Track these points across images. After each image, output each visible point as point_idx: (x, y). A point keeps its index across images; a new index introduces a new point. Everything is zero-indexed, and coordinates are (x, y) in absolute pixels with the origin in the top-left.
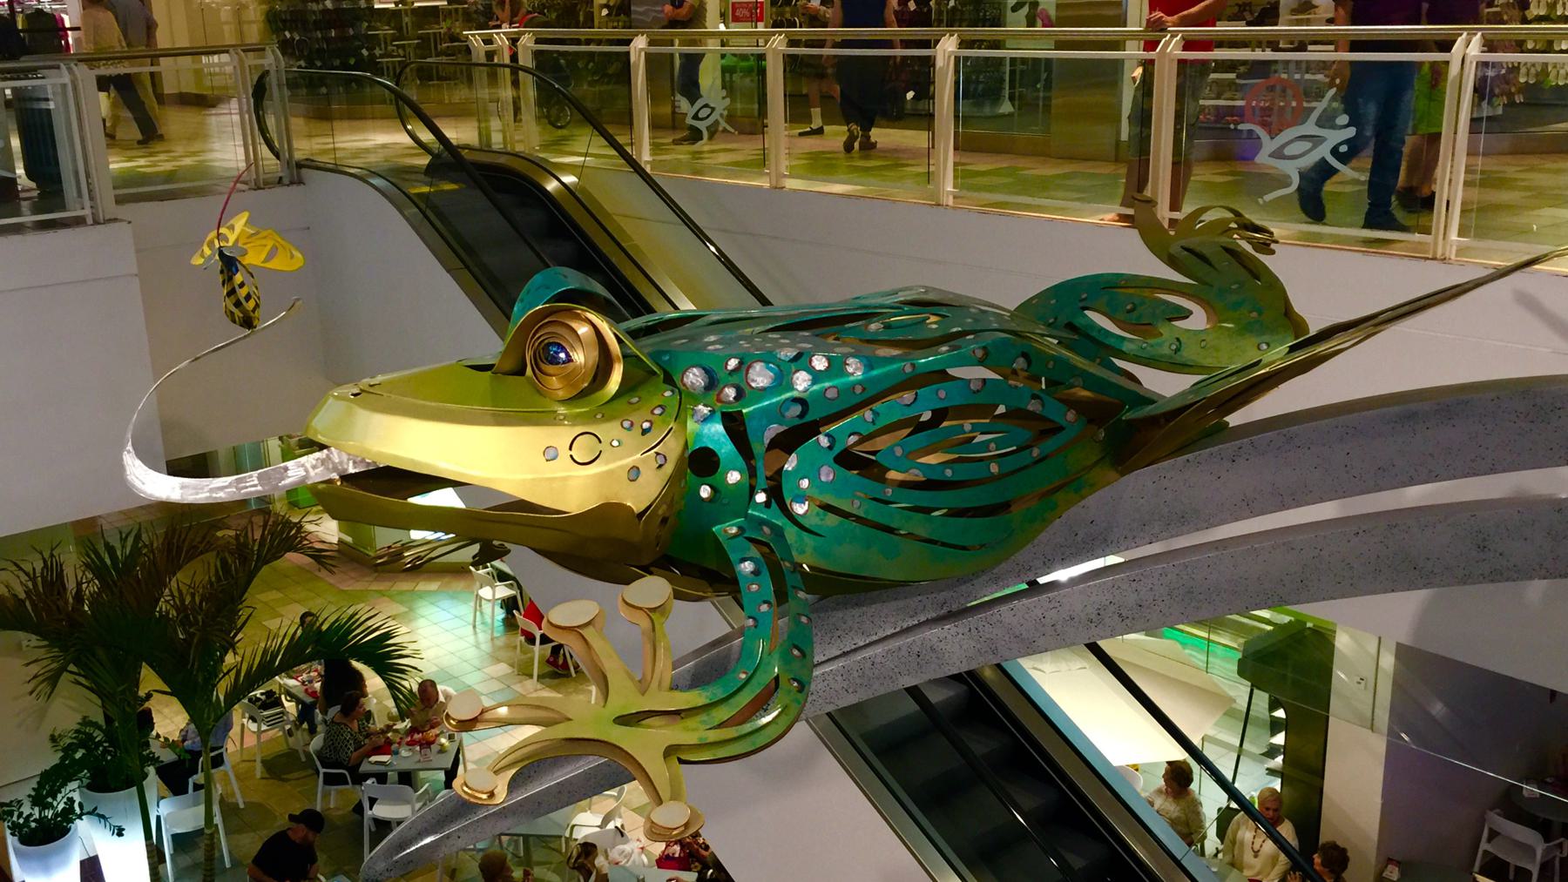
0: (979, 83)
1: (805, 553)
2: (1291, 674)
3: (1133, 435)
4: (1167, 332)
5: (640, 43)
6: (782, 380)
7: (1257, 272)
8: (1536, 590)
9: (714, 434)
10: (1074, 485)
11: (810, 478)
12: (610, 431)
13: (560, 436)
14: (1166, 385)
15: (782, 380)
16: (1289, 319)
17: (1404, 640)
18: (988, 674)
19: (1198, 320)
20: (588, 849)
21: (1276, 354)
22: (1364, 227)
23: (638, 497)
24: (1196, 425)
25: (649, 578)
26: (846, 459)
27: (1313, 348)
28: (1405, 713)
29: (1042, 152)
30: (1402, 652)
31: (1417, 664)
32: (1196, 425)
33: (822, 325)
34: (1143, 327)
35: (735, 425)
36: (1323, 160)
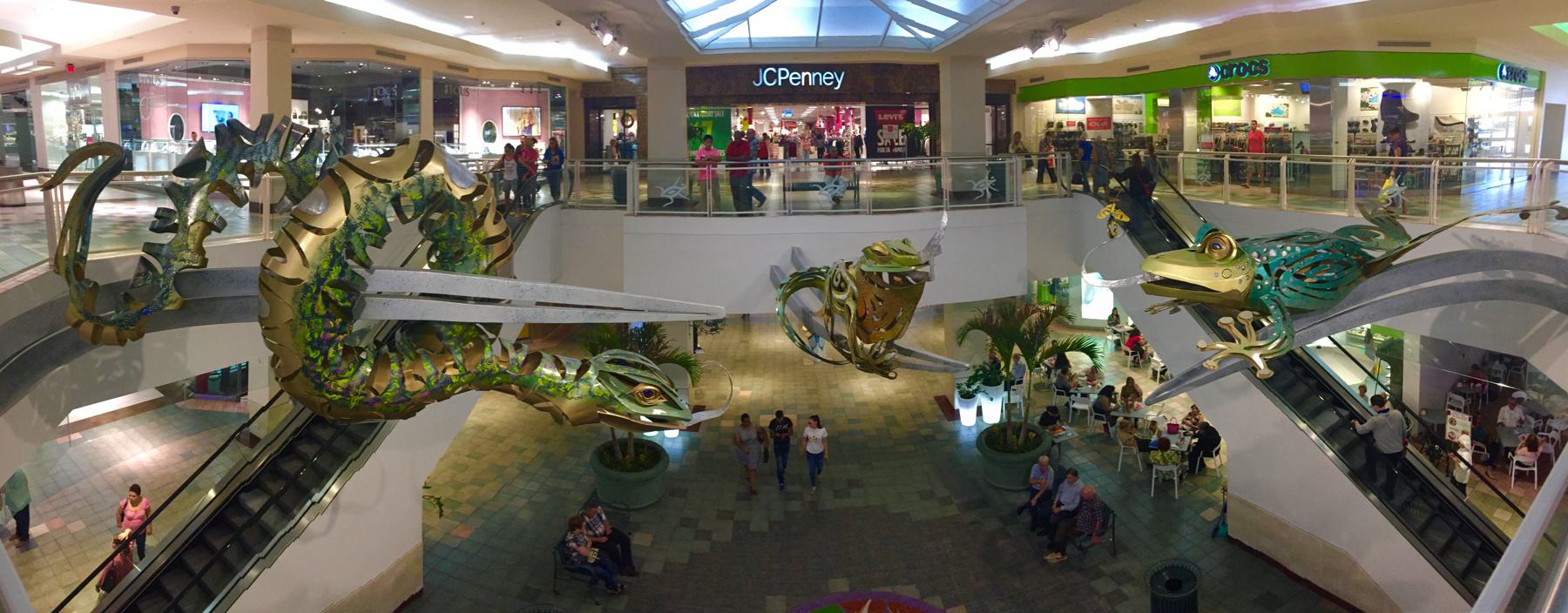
0: (1294, 170)
1: (1286, 302)
2: (1392, 353)
3: (1370, 268)
4: (1374, 240)
5: (1284, 159)
6: (1279, 254)
7: (1397, 224)
8: (1477, 305)
9: (1262, 271)
10: (1356, 282)
11: (1287, 280)
12: (1233, 268)
13: (1220, 270)
14: (1377, 254)
15: (1279, 254)
16: (1407, 236)
17: (1427, 334)
18: (1299, 352)
19: (1382, 236)
21: (1406, 244)
22: (660, 325)
23: (1242, 288)
24: (1384, 265)
25: (411, 540)
26: (1296, 276)
27: (1416, 243)
28: (1424, 359)
29: (1308, 194)
30: (1424, 339)
31: (1431, 345)
32: (1384, 265)
33: (1286, 238)
34: (1367, 239)
35: (1267, 267)
36: (1232, 181)
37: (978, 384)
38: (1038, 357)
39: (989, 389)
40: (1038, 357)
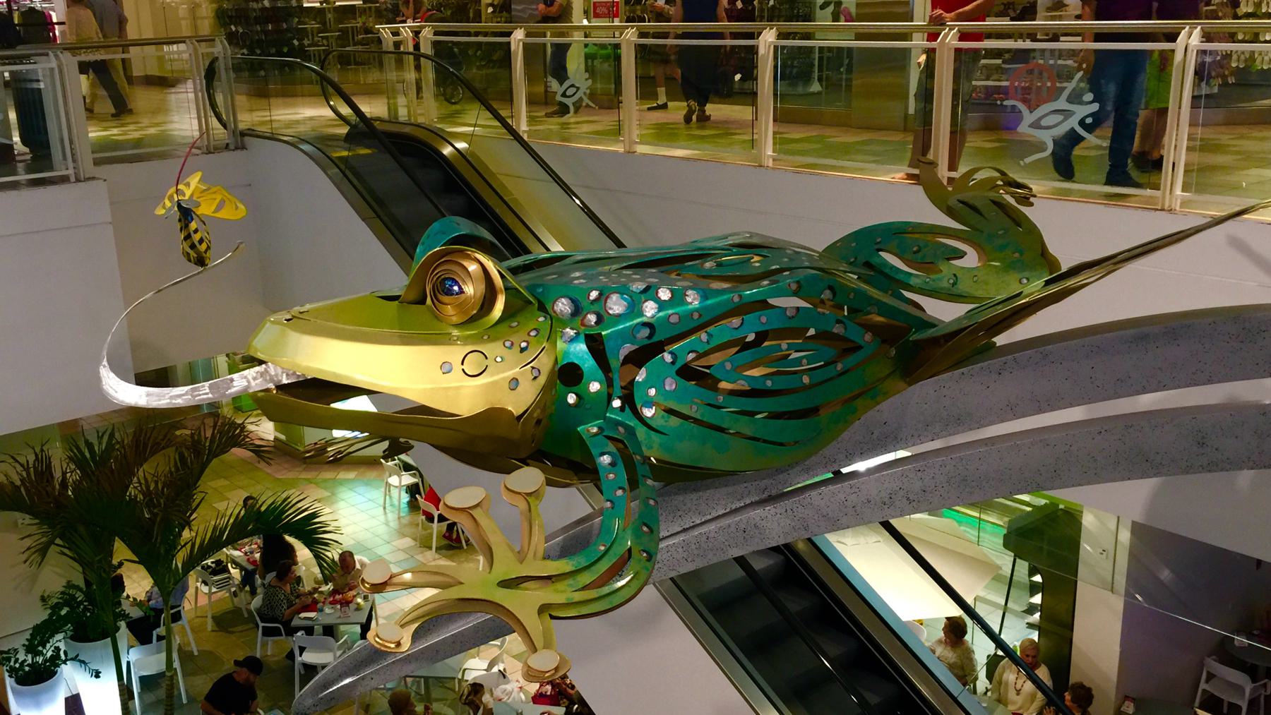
0: (794, 68)
1: (653, 448)
3: (919, 353)
4: (946, 269)
5: (519, 35)
6: (634, 308)
7: (1019, 221)
9: (579, 352)
10: (870, 393)
11: (656, 387)
12: (494, 349)
13: (454, 353)
14: (945, 312)
15: (634, 308)
16: (1045, 259)
17: (1138, 519)
19: (971, 259)
21: (1034, 287)
22: (1106, 184)
23: (518, 403)
24: (970, 345)
26: (686, 372)
27: (1064, 282)
28: (1139, 578)
29: (844, 123)
30: (1137, 529)
31: (1148, 538)
32: (970, 345)
33: (666, 263)
34: (926, 265)
35: (596, 345)
37: (59, 641)
38: (179, 561)
39: (86, 649)
40: (179, 561)
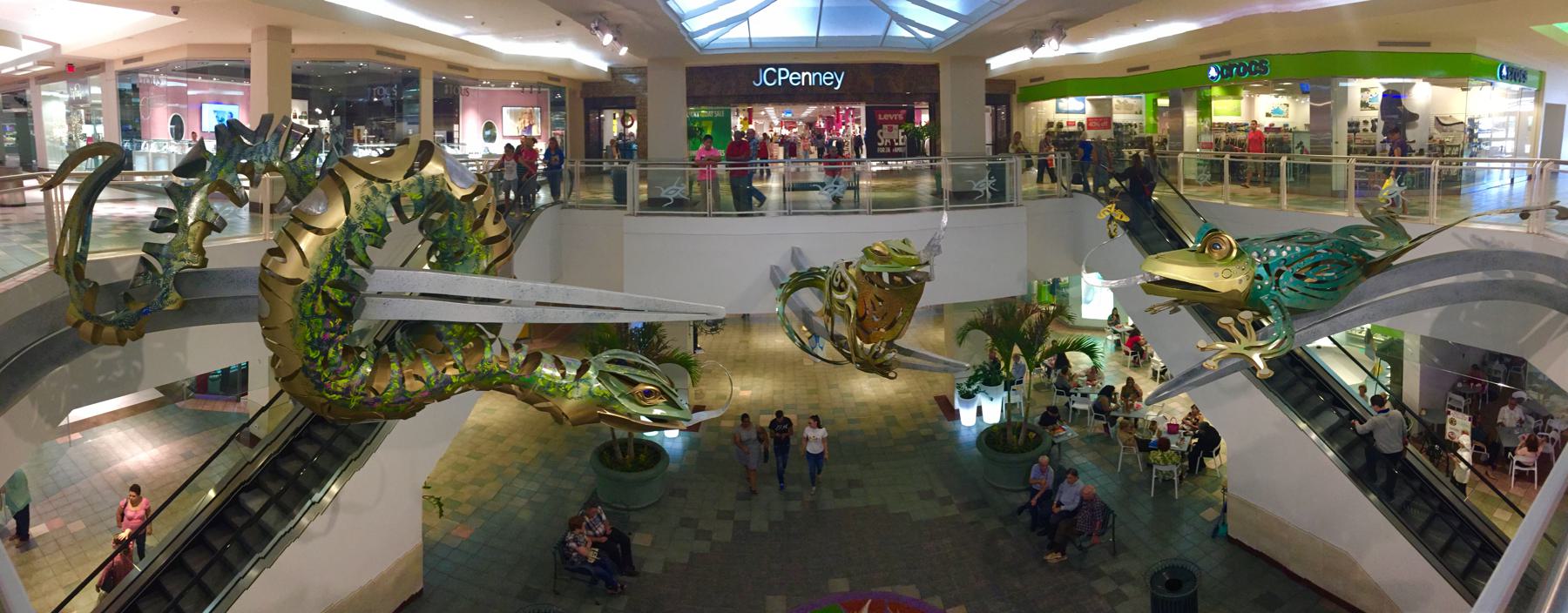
0: (1294, 170)
1: (1286, 302)
2: (1392, 353)
3: (1370, 268)
4: (1374, 240)
5: (1284, 159)
6: (1279, 254)
7: (1397, 224)
9: (1262, 271)
10: (1356, 282)
11: (1287, 280)
12: (1233, 268)
13: (1220, 270)
14: (1377, 254)
15: (1279, 254)
16: (1407, 236)
17: (1427, 334)
18: (1299, 352)
19: (1382, 236)
20: (1154, 423)
21: (1406, 244)
22: (660, 325)
23: (1242, 288)
24: (1384, 265)
26: (1296, 276)
27: (1416, 243)
28: (1424, 359)
29: (1308, 194)
30: (1424, 339)
31: (1431, 345)
32: (1384, 265)
33: (1286, 238)
34: (1367, 239)
35: (1267, 267)
37: (978, 384)
38: (1038, 357)
39: (989, 389)
40: (1038, 357)
